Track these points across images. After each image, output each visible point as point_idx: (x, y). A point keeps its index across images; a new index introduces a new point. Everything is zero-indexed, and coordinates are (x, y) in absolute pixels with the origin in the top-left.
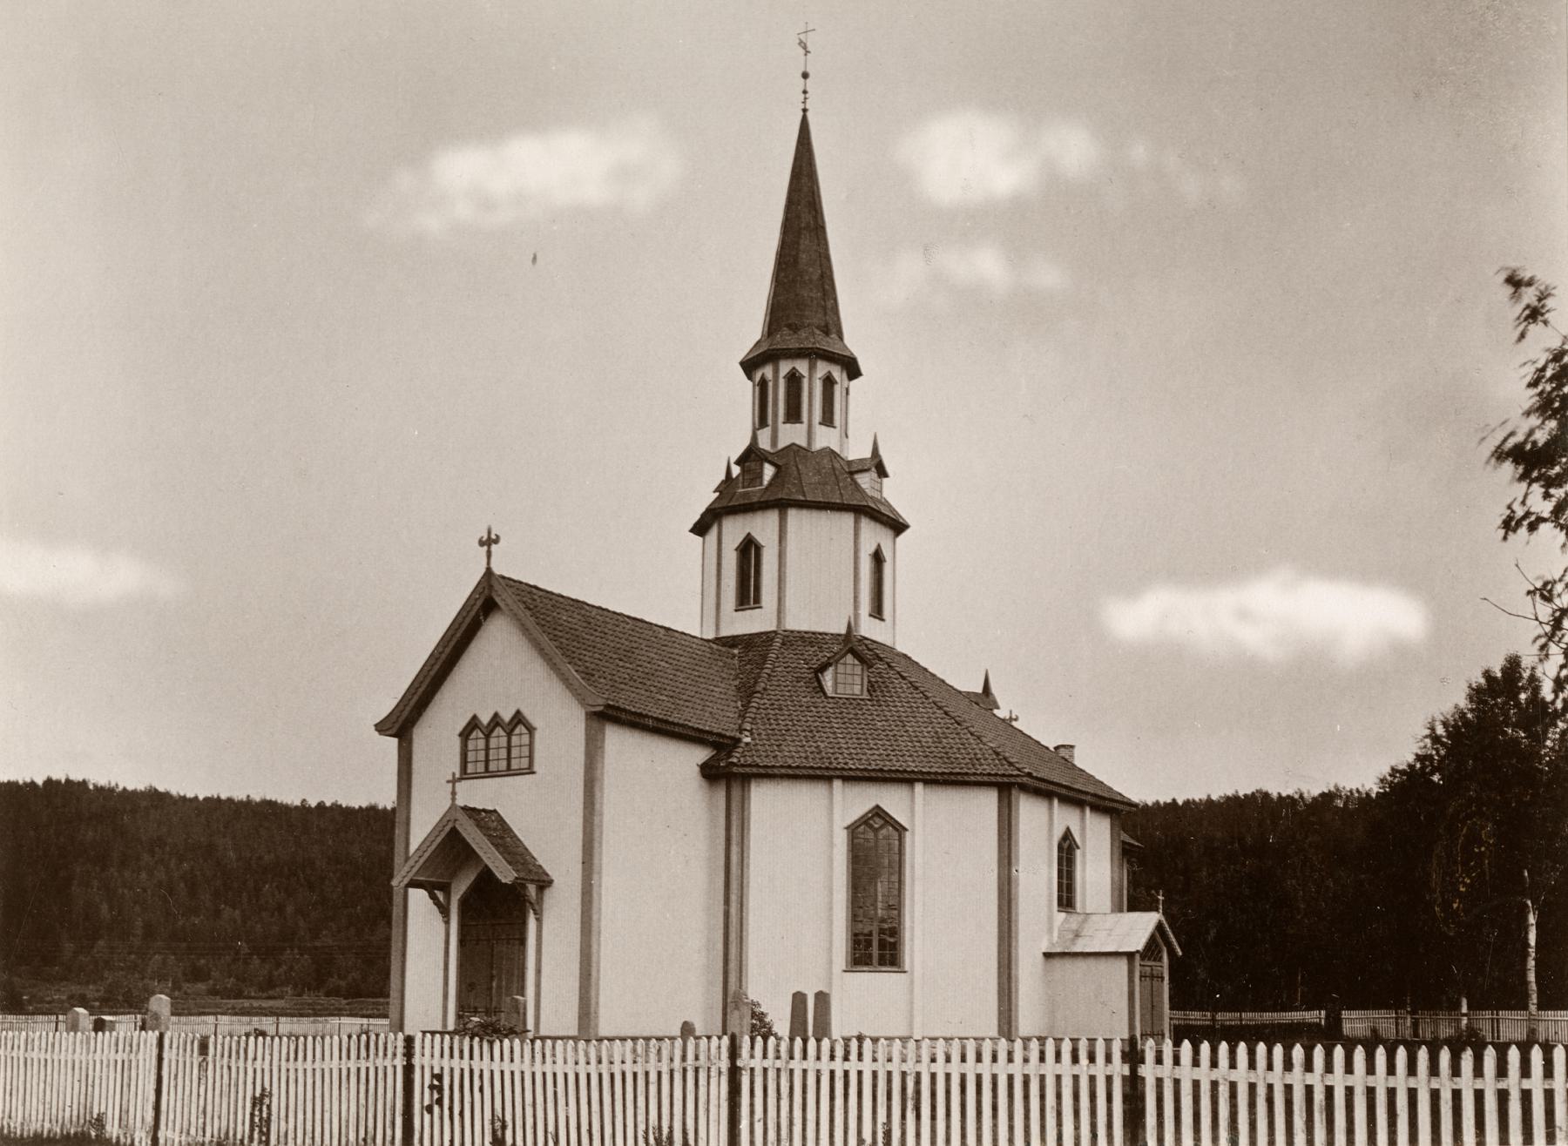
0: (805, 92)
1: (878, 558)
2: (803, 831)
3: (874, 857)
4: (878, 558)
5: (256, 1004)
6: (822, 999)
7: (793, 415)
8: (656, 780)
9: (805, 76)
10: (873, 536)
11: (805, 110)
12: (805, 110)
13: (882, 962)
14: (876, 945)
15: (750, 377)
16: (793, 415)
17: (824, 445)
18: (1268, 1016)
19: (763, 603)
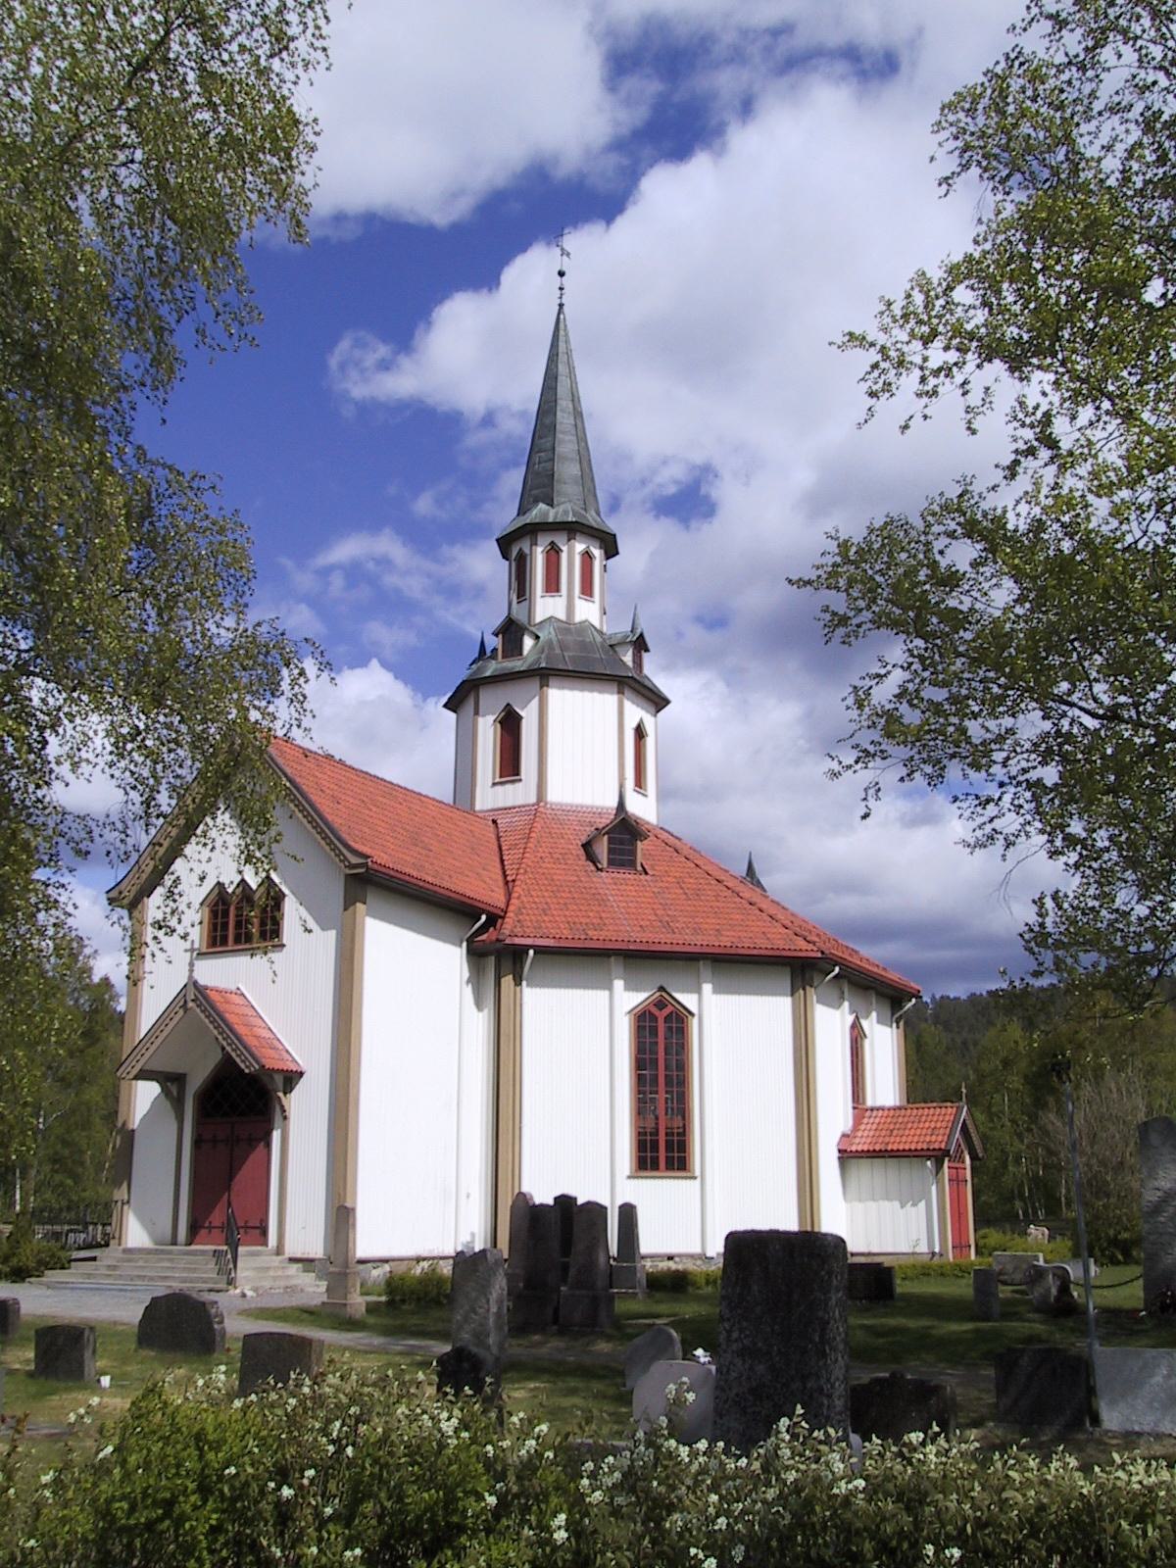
0: (561, 289)
1: (640, 733)
2: (580, 1029)
3: (661, 1061)
4: (640, 733)
5: (414, 1320)
6: (628, 1213)
7: (552, 585)
8: (414, 972)
9: (561, 274)
10: (635, 713)
11: (561, 306)
12: (561, 306)
13: (670, 1166)
14: (663, 1145)
15: (505, 556)
16: (552, 585)
17: (583, 618)
18: (912, 1324)
19: (523, 775)
